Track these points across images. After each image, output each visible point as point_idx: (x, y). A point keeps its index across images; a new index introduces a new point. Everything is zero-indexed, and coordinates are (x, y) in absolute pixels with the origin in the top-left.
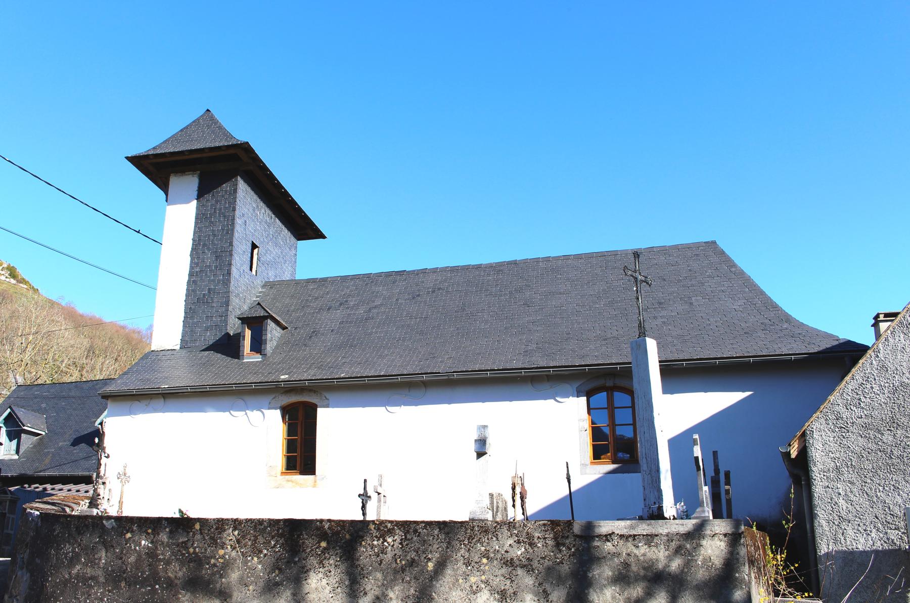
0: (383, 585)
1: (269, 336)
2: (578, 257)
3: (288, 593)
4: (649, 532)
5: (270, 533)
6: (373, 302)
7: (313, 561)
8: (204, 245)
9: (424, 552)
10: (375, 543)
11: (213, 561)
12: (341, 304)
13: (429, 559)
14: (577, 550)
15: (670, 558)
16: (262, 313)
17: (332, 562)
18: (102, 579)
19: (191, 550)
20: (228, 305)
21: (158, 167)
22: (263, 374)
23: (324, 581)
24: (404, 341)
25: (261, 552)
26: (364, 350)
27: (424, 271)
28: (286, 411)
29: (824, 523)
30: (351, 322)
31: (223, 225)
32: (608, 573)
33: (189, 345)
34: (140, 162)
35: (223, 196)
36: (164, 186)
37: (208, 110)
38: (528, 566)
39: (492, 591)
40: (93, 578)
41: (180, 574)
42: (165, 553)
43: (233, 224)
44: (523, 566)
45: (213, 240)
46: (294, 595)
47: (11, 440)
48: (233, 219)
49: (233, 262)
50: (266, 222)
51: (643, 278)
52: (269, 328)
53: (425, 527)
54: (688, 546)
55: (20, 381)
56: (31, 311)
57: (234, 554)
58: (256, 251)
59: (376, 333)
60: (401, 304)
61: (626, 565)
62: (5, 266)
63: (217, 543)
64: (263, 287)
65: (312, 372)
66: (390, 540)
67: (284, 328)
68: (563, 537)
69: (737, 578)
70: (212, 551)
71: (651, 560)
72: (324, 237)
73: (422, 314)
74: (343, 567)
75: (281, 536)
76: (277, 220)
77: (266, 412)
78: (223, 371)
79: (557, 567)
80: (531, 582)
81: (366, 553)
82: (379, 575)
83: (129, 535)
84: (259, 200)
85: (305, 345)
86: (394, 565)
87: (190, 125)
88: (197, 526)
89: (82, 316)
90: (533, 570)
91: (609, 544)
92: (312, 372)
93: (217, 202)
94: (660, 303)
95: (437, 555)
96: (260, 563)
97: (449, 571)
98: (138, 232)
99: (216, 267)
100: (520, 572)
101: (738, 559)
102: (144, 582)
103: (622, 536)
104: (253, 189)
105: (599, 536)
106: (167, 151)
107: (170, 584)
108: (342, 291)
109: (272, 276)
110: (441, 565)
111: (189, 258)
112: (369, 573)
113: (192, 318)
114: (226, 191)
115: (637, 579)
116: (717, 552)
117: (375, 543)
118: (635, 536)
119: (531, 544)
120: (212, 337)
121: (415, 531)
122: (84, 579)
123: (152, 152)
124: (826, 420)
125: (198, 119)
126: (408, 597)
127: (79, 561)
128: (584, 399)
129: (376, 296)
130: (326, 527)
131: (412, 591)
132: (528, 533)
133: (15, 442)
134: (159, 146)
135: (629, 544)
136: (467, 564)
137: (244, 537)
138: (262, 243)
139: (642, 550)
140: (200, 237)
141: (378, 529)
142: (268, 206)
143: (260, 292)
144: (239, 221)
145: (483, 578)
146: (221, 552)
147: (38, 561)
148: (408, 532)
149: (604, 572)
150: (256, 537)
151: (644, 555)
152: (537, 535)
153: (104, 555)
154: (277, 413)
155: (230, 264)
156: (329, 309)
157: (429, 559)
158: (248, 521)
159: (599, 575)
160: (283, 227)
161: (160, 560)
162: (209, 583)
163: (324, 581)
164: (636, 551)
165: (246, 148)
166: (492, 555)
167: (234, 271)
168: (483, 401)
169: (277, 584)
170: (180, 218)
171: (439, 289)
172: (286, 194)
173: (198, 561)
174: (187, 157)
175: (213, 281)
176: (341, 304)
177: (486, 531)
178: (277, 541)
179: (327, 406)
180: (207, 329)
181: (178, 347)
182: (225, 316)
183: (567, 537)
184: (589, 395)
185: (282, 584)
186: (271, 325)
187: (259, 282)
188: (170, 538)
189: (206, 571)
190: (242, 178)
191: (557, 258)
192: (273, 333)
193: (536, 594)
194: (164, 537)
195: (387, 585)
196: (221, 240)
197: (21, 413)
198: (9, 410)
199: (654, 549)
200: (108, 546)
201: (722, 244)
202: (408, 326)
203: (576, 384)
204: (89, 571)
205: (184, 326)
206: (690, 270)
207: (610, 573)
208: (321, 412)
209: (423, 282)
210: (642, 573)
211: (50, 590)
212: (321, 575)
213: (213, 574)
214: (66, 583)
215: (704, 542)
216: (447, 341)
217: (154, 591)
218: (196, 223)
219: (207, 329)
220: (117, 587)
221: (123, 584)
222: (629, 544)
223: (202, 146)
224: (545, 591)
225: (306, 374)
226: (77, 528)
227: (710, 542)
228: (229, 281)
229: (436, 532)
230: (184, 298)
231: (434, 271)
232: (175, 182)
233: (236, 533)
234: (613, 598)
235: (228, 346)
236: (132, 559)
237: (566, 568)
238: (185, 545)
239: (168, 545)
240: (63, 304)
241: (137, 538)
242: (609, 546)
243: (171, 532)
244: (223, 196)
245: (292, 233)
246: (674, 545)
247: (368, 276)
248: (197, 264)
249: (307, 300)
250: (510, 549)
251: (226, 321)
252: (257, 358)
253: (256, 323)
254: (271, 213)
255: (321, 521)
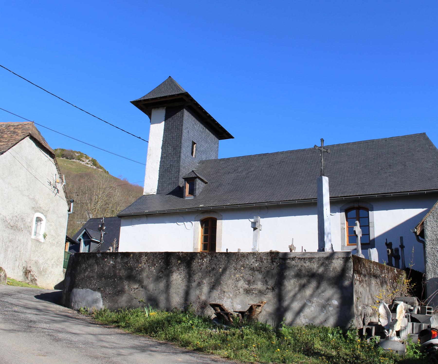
0: (202, 278)
1: (197, 186)
2: (354, 143)
3: (165, 281)
4: (311, 257)
5: (159, 257)
6: (250, 169)
7: (175, 268)
8: (168, 143)
9: (218, 265)
10: (199, 261)
11: (137, 269)
12: (235, 171)
13: (220, 268)
14: (280, 264)
15: (319, 267)
16: (194, 176)
17: (182, 269)
18: (96, 277)
19: (129, 265)
20: (179, 173)
21: (147, 106)
22: (192, 204)
23: (179, 276)
24: (261, 188)
25: (155, 265)
26: (242, 192)
27: (277, 153)
28: (204, 223)
29: (430, 265)
30: (238, 179)
31: (177, 133)
32: (293, 273)
33: (161, 192)
34: (137, 103)
35: (177, 119)
36: (149, 114)
37: (170, 77)
38: (259, 270)
39: (245, 280)
40: (92, 277)
41: (125, 274)
42: (119, 266)
43: (182, 133)
44: (258, 271)
45: (172, 141)
46: (167, 282)
47: (86, 246)
48: (182, 130)
49: (182, 151)
50: (200, 131)
51: (325, 150)
52: (197, 183)
53: (219, 255)
54: (327, 262)
55: (91, 216)
56: (100, 182)
57: (145, 266)
58: (195, 146)
59: (249, 184)
60: (263, 170)
61: (300, 270)
62: (91, 159)
63: (138, 262)
64: (199, 163)
65: (215, 203)
66: (205, 260)
67: (206, 183)
68: (275, 259)
69: (347, 276)
70: (137, 265)
71: (311, 268)
72: (233, 138)
73: (272, 174)
74: (186, 271)
75: (163, 259)
76: (207, 130)
77: (193, 222)
78: (176, 203)
79: (271, 271)
80: (261, 277)
81: (195, 265)
82: (200, 274)
83: (106, 260)
84: (196, 120)
85: (215, 191)
86: (206, 270)
87: (161, 84)
88: (132, 255)
89: (131, 185)
90: (262, 272)
91: (293, 261)
92: (215, 203)
93: (174, 122)
94: (390, 166)
95: (224, 266)
96: (155, 269)
97: (228, 272)
98: (140, 138)
99: (174, 154)
100: (256, 273)
101: (348, 268)
102: (111, 278)
103: (299, 258)
104: (192, 115)
105: (290, 258)
106: (150, 98)
107: (121, 278)
108: (236, 164)
109: (204, 158)
110: (225, 270)
111: (161, 150)
112: (196, 273)
113: (162, 179)
114: (178, 116)
115: (305, 276)
116: (339, 265)
117: (199, 261)
118: (305, 258)
119: (261, 262)
120: (171, 188)
121: (216, 256)
122: (89, 277)
123: (142, 99)
124: (433, 216)
125: (165, 81)
126: (211, 282)
127: (88, 270)
128: (343, 214)
129: (252, 167)
130: (181, 255)
131: (213, 280)
132: (260, 257)
133: (88, 246)
134: (146, 95)
135: (302, 262)
136: (235, 269)
137: (149, 259)
138: (198, 141)
139: (307, 264)
140: (166, 139)
141: (201, 256)
142: (201, 123)
143: (197, 166)
144: (185, 131)
145: (241, 275)
146: (140, 265)
147: (73, 272)
148: (213, 257)
149: (290, 273)
150: (154, 259)
151: (308, 266)
152: (264, 258)
153: (97, 267)
154: (199, 222)
155: (180, 152)
156: (228, 173)
157: (220, 268)
158: (151, 253)
159: (289, 274)
160: (211, 133)
161: (117, 269)
162: (135, 277)
163: (179, 276)
164: (305, 264)
165: (187, 95)
166: (245, 266)
167: (182, 155)
168: (295, 216)
169: (161, 278)
170: (157, 131)
171: (283, 162)
172: (210, 117)
173: (131, 269)
174: (175, 98)
175: (172, 161)
176: (235, 171)
177: (244, 256)
178: (162, 261)
179: (222, 219)
180: (169, 184)
181: (155, 193)
182: (177, 178)
183: (277, 259)
184: (347, 212)
185: (162, 278)
186: (198, 182)
187: (196, 161)
188: (121, 260)
189: (134, 272)
190: (186, 109)
191: (343, 145)
192: (199, 186)
193: (262, 282)
194: (119, 260)
195: (202, 278)
196: (176, 141)
197: (90, 232)
198: (85, 230)
199: (312, 264)
200: (98, 264)
201: (428, 135)
202: (265, 180)
203: (340, 206)
204: (91, 274)
205: (159, 183)
206: (409, 148)
207: (293, 274)
208: (219, 222)
209: (276, 159)
210: (307, 273)
211: (77, 282)
212: (178, 274)
213: (137, 274)
214: (82, 279)
215: (334, 261)
216: (279, 188)
217: (115, 281)
218: (164, 133)
219: (169, 184)
220: (101, 280)
221: (103, 279)
222: (302, 262)
223: (166, 95)
224: (266, 281)
225: (211, 204)
226: (87, 258)
227: (336, 261)
228: (180, 160)
229: (224, 257)
230: (159, 169)
231: (282, 153)
232: (154, 113)
233: (146, 258)
234: (294, 283)
235: (178, 192)
236: (107, 269)
237: (275, 271)
238: (127, 263)
239: (120, 263)
240: (122, 179)
241: (109, 261)
242: (293, 262)
243: (122, 258)
244: (177, 119)
245: (215, 136)
246: (321, 262)
247: (250, 156)
248: (165, 153)
249: (219, 169)
250: (253, 264)
251: (178, 180)
252: (192, 197)
253: (191, 180)
254: (203, 126)
255: (179, 252)
